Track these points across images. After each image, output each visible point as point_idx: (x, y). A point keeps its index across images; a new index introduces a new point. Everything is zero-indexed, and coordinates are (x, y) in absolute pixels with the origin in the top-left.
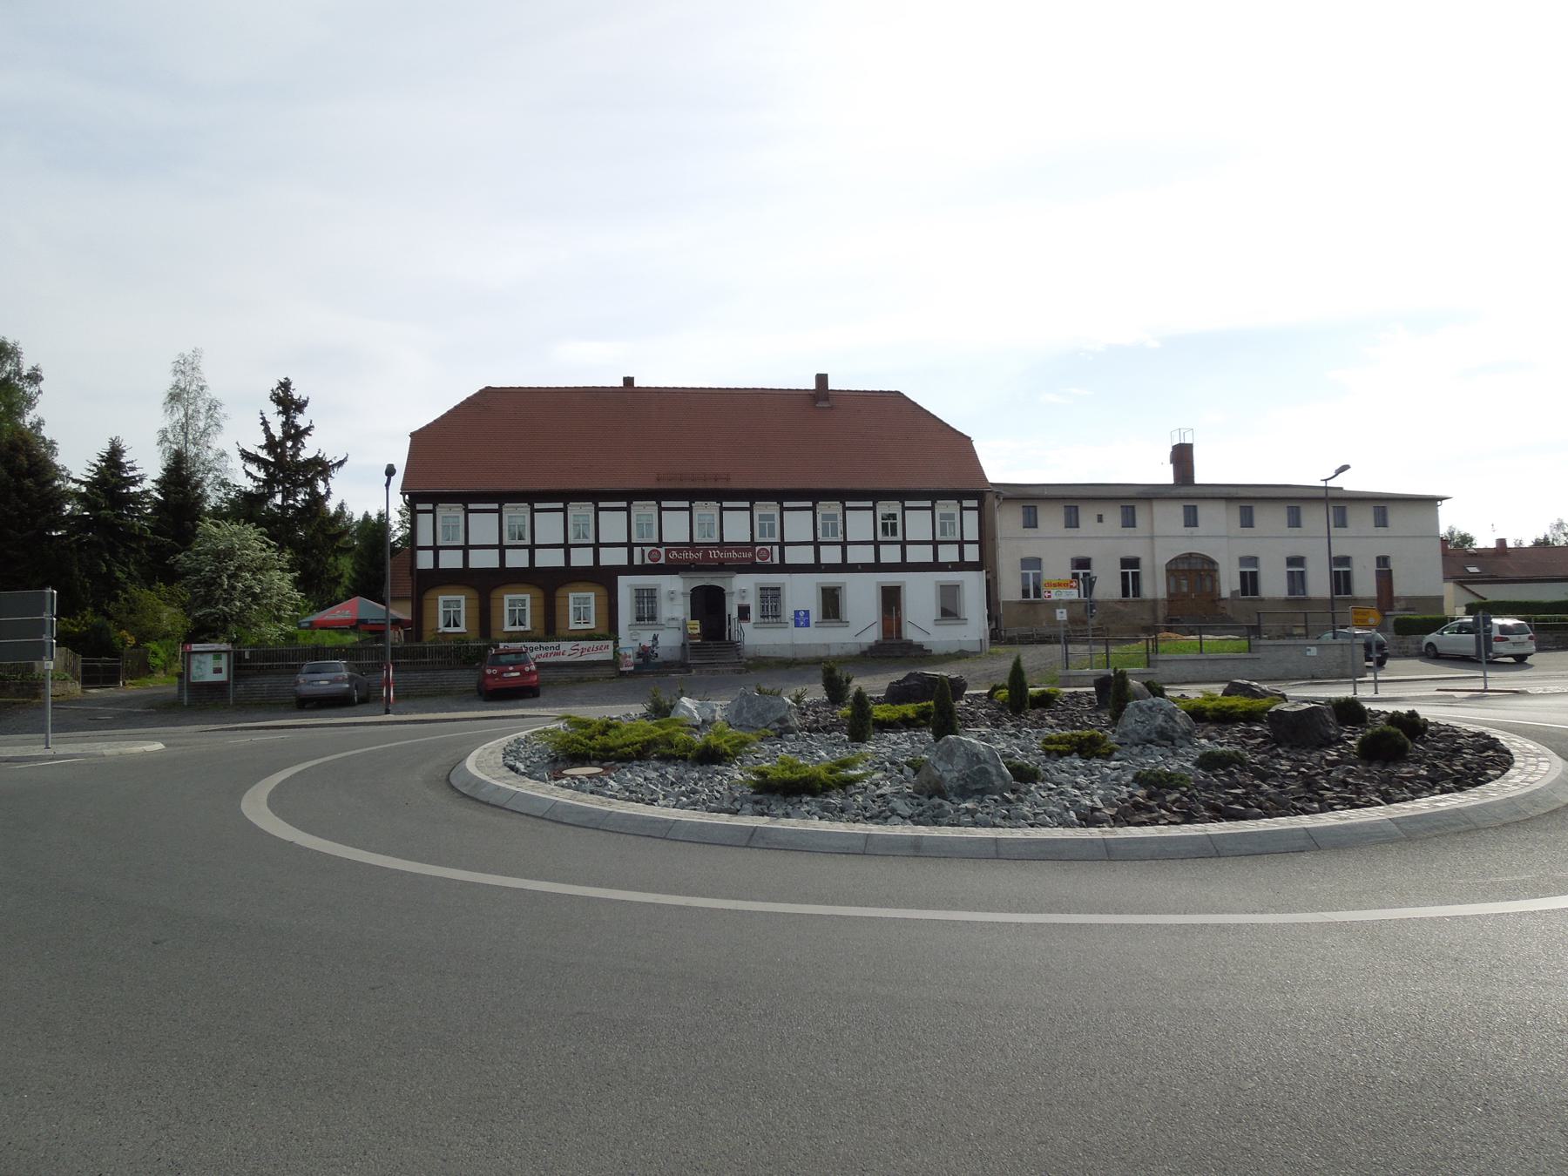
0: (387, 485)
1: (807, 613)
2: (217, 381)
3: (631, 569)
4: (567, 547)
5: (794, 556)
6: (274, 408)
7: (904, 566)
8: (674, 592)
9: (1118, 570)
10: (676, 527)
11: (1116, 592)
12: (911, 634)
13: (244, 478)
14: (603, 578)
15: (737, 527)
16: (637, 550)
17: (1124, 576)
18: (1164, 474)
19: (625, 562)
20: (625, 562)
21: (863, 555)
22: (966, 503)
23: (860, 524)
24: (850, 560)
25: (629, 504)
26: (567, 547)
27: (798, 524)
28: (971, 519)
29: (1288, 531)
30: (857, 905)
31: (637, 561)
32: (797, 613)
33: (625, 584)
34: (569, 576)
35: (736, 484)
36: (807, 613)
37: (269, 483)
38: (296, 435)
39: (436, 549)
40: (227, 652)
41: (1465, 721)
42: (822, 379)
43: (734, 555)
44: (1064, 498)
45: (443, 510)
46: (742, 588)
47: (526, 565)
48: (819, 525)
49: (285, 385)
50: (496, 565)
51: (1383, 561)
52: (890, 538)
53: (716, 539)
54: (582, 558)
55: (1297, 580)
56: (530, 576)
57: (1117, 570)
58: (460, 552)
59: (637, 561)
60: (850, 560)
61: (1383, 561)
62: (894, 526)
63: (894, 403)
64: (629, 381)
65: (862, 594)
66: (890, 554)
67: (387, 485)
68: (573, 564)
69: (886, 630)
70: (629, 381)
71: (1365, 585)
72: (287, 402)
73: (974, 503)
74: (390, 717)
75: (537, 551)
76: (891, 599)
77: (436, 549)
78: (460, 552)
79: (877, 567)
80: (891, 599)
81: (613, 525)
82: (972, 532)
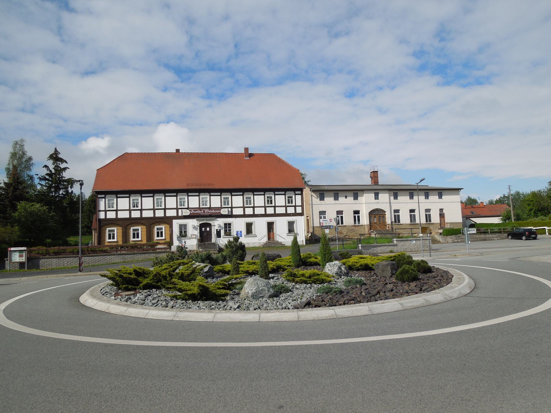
0: (81, 189)
1: (241, 232)
2: (30, 151)
3: (177, 217)
4: (154, 210)
5: (236, 212)
6: (51, 161)
7: (275, 215)
8: (192, 225)
9: (352, 215)
10: (194, 202)
11: (408, 222)
12: (278, 239)
13: (39, 186)
14: (167, 221)
15: (215, 201)
16: (180, 211)
17: (355, 217)
18: (368, 181)
19: (176, 215)
20: (176, 215)
21: (261, 211)
22: (297, 192)
23: (259, 200)
24: (288, 212)
25: (177, 194)
26: (154, 210)
27: (237, 200)
28: (299, 197)
29: (334, 202)
30: (154, 346)
31: (180, 214)
32: (237, 232)
33: (176, 223)
34: (131, 221)
35: (249, 187)
36: (241, 232)
37: (50, 187)
38: (59, 171)
39: (106, 211)
40: (25, 250)
41: (442, 265)
42: (246, 149)
43: (214, 211)
44: (389, 190)
45: (108, 197)
46: (217, 224)
47: (139, 216)
48: (245, 201)
49: (56, 152)
50: (152, 216)
51: (441, 210)
52: (290, 205)
53: (208, 206)
54: (160, 214)
55: (428, 218)
56: (140, 221)
57: (352, 215)
58: (176, 210)
59: (180, 214)
60: (288, 212)
61: (441, 210)
62: (271, 201)
63: (271, 157)
64: (178, 151)
65: (260, 225)
66: (249, 211)
67: (81, 189)
68: (156, 216)
69: (269, 238)
70: (178, 151)
71: (435, 219)
72: (55, 157)
73: (300, 192)
74: (92, 273)
75: (255, 208)
76: (270, 226)
77: (106, 211)
78: (176, 210)
79: (266, 215)
80: (270, 226)
81: (171, 202)
82: (299, 203)
